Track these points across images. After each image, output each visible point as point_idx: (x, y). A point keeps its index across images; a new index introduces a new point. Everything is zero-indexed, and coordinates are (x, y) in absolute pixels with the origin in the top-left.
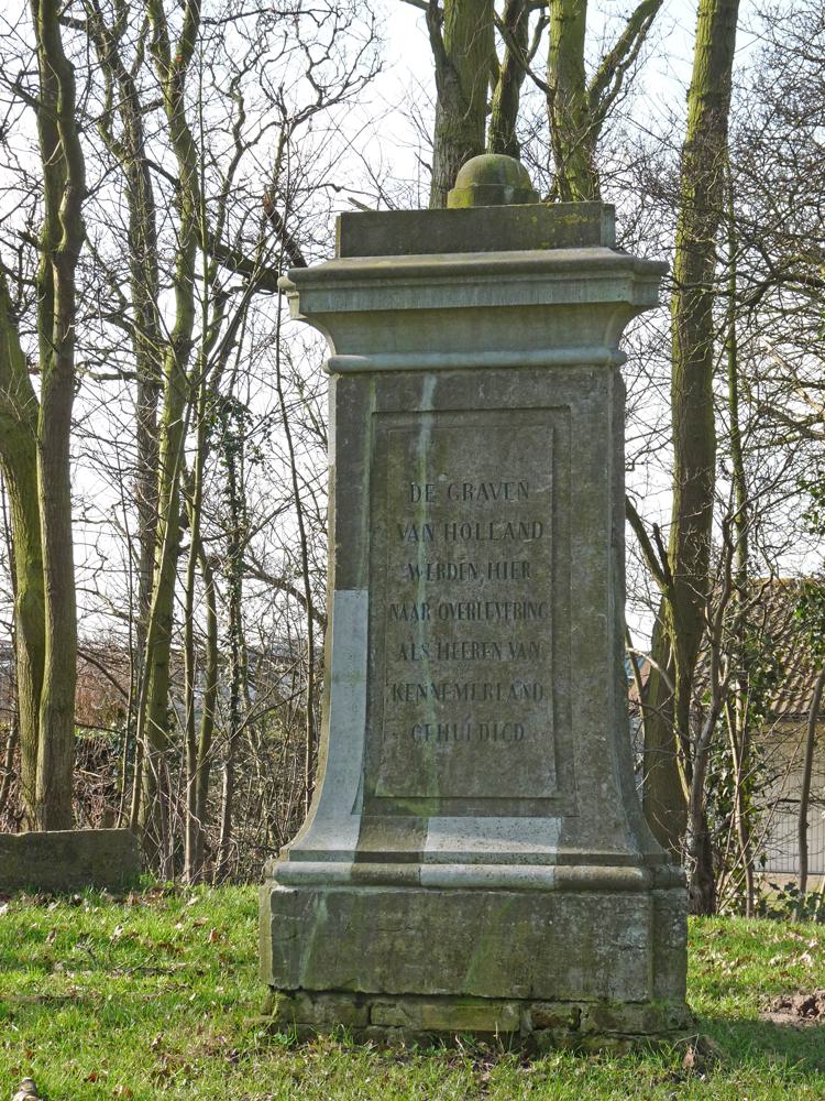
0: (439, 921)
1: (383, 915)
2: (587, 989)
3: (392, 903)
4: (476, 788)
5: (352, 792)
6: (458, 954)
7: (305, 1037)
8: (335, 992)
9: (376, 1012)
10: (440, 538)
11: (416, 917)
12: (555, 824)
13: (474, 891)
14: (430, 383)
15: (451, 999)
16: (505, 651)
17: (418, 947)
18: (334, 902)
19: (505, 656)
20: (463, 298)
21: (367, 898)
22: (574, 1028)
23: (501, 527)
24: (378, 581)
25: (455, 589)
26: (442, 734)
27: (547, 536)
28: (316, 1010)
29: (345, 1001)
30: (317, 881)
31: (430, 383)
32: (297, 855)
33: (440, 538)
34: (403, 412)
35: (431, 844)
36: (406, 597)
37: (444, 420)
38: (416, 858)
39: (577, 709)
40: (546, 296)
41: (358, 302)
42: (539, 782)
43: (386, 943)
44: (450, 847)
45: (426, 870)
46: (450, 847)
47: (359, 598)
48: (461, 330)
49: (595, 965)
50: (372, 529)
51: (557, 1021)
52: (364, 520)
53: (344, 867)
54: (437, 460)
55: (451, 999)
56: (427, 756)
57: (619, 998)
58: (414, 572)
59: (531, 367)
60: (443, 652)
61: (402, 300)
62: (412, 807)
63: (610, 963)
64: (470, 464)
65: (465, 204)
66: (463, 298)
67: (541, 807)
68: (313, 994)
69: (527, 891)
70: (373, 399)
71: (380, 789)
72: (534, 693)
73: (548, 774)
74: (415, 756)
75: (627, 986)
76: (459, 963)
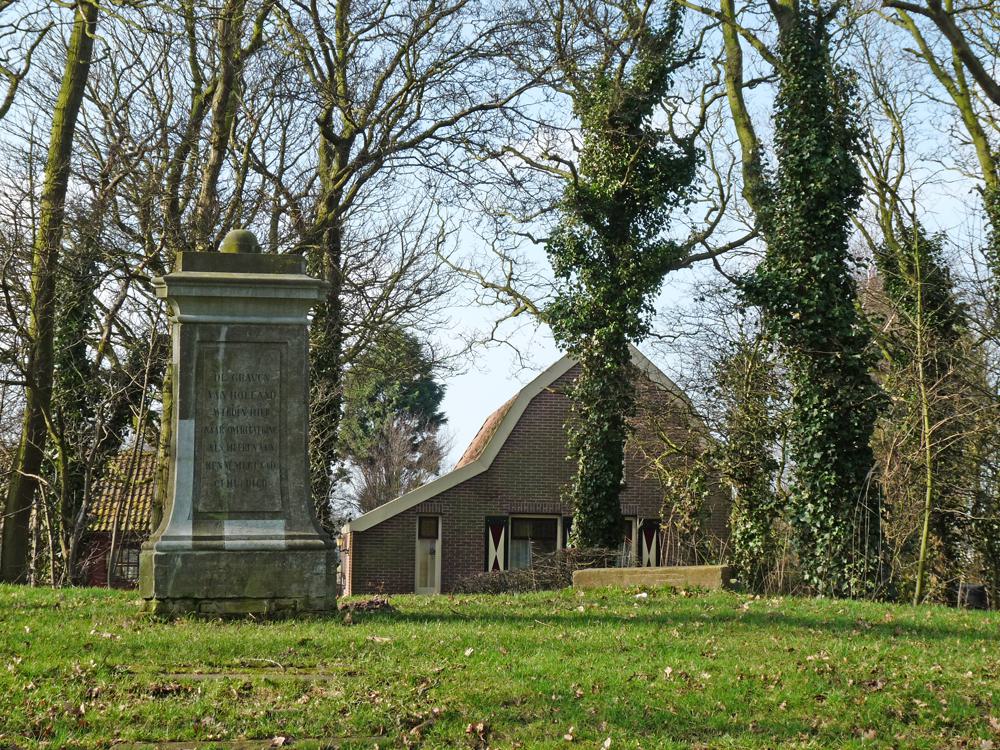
0: (233, 565)
1: (208, 563)
2: (300, 592)
3: (213, 558)
4: (245, 507)
5: (188, 510)
6: (242, 580)
7: (172, 619)
8: (184, 598)
9: (204, 607)
10: (228, 398)
11: (223, 564)
12: (282, 522)
13: (249, 553)
14: (224, 330)
15: (238, 599)
16: (258, 448)
17: (224, 577)
18: (185, 558)
19: (258, 450)
20: (244, 293)
21: (201, 556)
22: (294, 609)
23: (256, 393)
24: (199, 417)
25: (235, 420)
26: (229, 484)
27: (277, 398)
28: (174, 608)
29: (188, 602)
30: (175, 549)
31: (224, 330)
32: (165, 538)
33: (228, 398)
34: (212, 342)
35: (227, 532)
36: (213, 423)
37: (230, 346)
38: (221, 538)
39: (290, 473)
40: (282, 294)
41: (195, 292)
42: (274, 504)
43: (209, 576)
44: (235, 533)
45: (227, 543)
46: (235, 533)
47: (191, 424)
48: (240, 307)
49: (304, 582)
50: (197, 393)
51: (287, 607)
52: (193, 389)
53: (189, 543)
54: (227, 363)
55: (238, 599)
56: (222, 494)
57: (314, 595)
58: (216, 412)
59: (270, 324)
60: (230, 448)
61: (216, 292)
62: (216, 516)
63: (310, 581)
64: (243, 365)
65: (233, 251)
66: (244, 293)
67: (274, 515)
68: (174, 600)
69: (274, 553)
70: (198, 335)
71: (200, 508)
72: (271, 466)
73: (278, 501)
74: (217, 494)
75: (316, 592)
76: (243, 582)
